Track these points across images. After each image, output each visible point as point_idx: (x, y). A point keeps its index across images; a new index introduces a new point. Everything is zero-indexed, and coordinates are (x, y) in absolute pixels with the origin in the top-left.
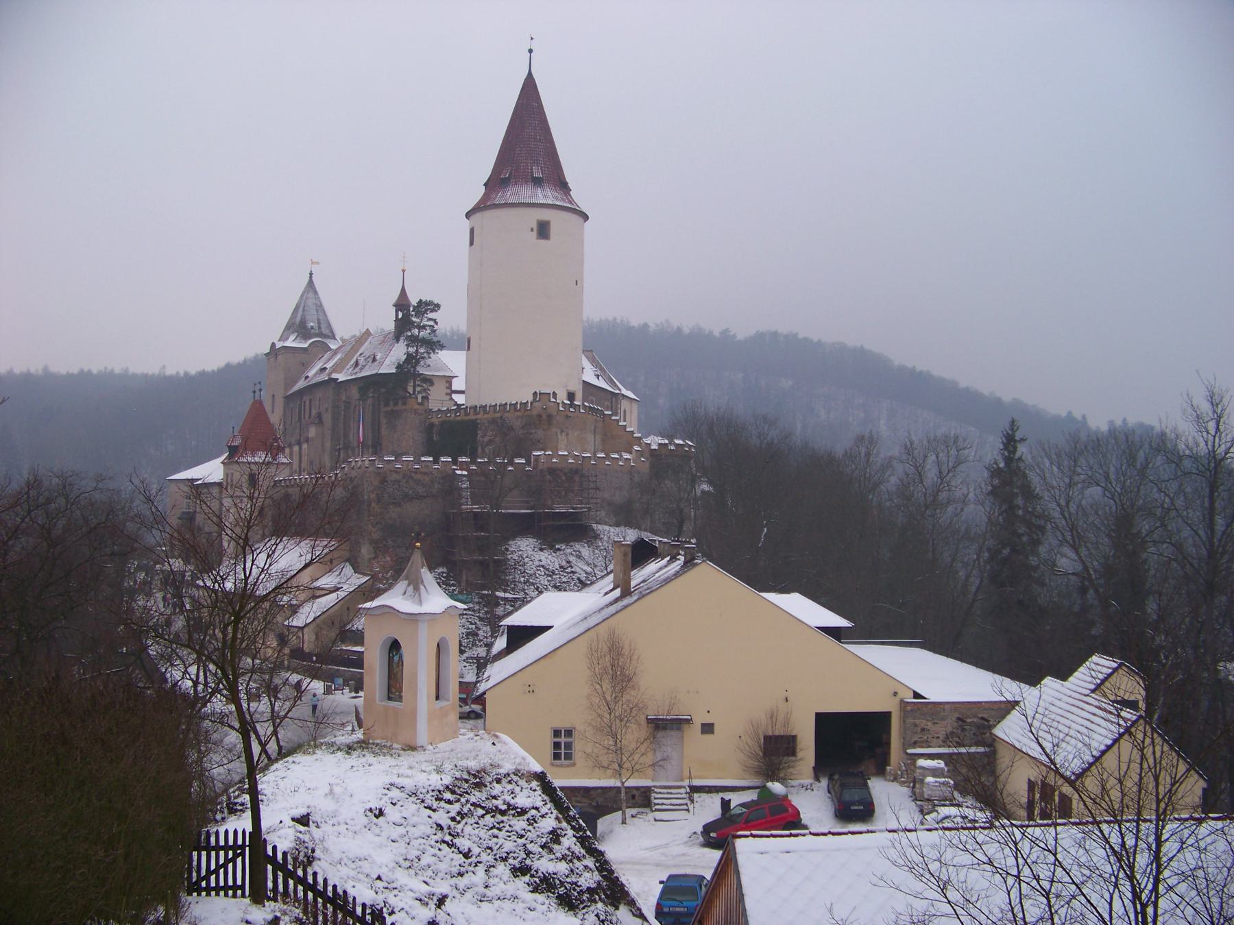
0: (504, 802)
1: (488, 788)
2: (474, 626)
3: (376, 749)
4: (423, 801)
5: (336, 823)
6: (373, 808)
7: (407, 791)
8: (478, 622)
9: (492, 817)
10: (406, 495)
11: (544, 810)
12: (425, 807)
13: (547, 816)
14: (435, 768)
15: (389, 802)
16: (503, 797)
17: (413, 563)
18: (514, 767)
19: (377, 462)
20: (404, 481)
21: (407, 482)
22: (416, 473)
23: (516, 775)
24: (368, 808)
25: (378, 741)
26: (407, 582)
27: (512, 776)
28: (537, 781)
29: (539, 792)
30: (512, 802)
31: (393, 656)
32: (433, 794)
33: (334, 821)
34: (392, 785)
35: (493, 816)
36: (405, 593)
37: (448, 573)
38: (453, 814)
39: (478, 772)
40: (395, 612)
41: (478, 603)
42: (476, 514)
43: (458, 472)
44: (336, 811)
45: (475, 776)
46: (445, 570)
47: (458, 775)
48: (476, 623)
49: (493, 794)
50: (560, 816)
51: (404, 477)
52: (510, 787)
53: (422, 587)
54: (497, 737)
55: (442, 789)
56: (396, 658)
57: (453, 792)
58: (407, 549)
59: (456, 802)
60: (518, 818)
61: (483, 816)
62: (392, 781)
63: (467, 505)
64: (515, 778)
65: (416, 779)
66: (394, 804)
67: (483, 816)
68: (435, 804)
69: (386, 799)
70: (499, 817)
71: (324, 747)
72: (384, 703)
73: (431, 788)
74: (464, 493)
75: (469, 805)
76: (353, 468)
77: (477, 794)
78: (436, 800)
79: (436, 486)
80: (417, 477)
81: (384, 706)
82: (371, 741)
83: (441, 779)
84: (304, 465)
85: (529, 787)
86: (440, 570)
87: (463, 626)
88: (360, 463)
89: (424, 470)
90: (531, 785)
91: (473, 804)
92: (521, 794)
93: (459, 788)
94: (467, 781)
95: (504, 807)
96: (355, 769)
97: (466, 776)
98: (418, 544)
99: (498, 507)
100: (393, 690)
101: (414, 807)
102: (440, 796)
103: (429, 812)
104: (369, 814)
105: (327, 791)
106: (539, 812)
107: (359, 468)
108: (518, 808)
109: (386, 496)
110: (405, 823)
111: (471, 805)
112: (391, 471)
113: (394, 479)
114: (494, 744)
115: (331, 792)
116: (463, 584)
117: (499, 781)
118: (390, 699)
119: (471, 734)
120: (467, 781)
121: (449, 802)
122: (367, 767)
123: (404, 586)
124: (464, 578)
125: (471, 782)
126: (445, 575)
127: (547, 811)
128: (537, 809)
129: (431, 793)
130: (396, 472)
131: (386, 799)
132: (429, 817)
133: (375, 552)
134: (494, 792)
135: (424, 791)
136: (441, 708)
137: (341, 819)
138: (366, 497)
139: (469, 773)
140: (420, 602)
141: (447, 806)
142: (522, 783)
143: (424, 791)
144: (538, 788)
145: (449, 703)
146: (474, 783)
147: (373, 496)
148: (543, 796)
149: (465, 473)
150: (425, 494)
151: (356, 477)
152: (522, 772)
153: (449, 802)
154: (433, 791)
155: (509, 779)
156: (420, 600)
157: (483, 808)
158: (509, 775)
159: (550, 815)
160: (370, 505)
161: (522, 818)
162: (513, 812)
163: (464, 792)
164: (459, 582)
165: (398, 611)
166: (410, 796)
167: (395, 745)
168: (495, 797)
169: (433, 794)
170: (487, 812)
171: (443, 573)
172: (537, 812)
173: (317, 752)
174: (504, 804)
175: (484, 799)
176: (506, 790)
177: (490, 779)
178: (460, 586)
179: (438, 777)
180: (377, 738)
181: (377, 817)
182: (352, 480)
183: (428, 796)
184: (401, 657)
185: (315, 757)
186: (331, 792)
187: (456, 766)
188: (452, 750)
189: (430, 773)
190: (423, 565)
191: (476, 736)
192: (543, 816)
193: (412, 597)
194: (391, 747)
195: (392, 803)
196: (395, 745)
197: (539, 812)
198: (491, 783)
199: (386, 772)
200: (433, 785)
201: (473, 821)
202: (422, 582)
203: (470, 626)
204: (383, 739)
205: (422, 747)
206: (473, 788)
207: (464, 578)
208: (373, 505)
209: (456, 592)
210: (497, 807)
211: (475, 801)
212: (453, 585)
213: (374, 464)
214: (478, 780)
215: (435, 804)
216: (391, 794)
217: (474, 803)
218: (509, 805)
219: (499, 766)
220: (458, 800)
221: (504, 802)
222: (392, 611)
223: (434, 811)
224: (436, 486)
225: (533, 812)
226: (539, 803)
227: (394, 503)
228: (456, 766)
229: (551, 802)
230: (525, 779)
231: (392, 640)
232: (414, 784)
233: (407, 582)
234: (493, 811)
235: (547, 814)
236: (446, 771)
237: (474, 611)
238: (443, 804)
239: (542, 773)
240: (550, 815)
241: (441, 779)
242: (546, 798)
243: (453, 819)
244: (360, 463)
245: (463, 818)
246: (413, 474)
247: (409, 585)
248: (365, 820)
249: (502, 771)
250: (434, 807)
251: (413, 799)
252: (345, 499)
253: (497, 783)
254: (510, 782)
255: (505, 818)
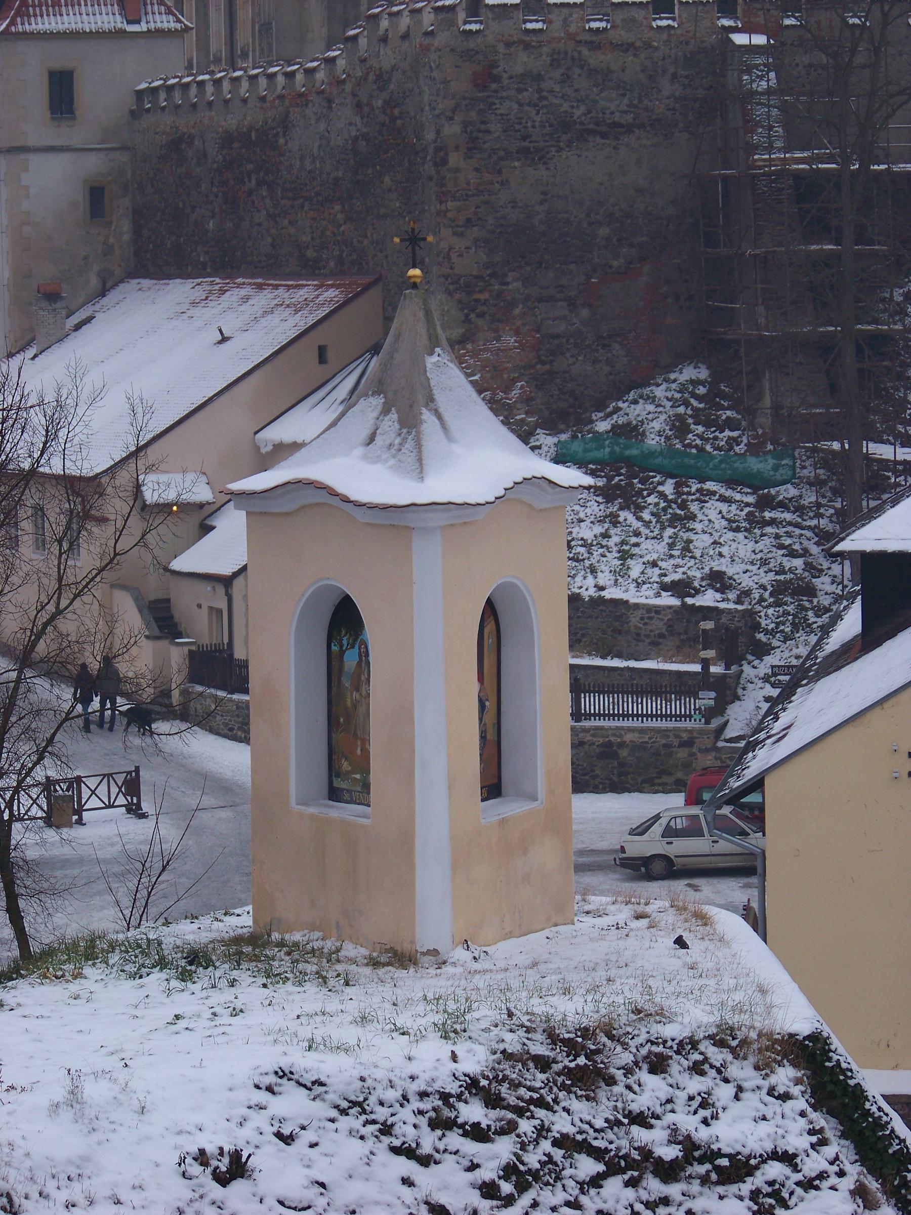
0: (675, 1136)
1: (619, 1089)
2: (798, 563)
3: (282, 963)
4: (386, 1130)
5: (79, 1198)
6: (211, 1149)
7: (331, 1097)
8: (814, 550)
9: (627, 1184)
10: (565, 125)
11: (813, 1164)
12: (396, 1150)
13: (825, 1184)
14: (439, 1018)
15: (269, 1130)
16: (669, 1118)
17: (398, 336)
18: (714, 1018)
19: (461, 15)
20: (557, 74)
21: (566, 79)
22: (594, 47)
23: (720, 1044)
24: (194, 1149)
25: (297, 937)
26: (377, 402)
27: (708, 1048)
28: (795, 1065)
29: (801, 1104)
30: (702, 1134)
31: (342, 652)
32: (423, 1106)
33: (76, 1192)
34: (282, 1074)
35: (632, 1183)
36: (371, 439)
37: (713, 383)
38: (488, 1173)
39: (585, 1032)
40: (335, 501)
41: (816, 483)
42: (798, 176)
43: (740, 39)
44: (86, 1159)
45: (572, 1048)
46: (703, 373)
47: (513, 1042)
48: (806, 552)
49: (635, 1107)
50: (873, 1185)
51: (555, 63)
52: (695, 1085)
53: (427, 416)
54: (703, 919)
55: (453, 1088)
56: (351, 659)
57: (493, 1101)
58: (572, 305)
59: (502, 1132)
60: (720, 1189)
61: (596, 1181)
62: (285, 1063)
63: (770, 149)
64: (717, 1055)
65: (366, 1056)
66: (287, 1139)
67: (596, 1181)
68: (428, 1141)
69: (259, 1120)
70: (654, 1186)
71: (114, 958)
72: (312, 810)
73: (414, 1088)
74: (761, 111)
75: (546, 1145)
76: (384, 40)
77: (578, 1106)
78: (434, 1124)
79: (667, 88)
80: (597, 59)
81: (313, 817)
82: (275, 936)
83: (454, 1057)
84: (244, 36)
85: (766, 1084)
86: (688, 373)
87: (764, 562)
88: (405, 21)
89: (621, 36)
90: (773, 1079)
91: (562, 1141)
92: (736, 1109)
93: (515, 1085)
94: (543, 1064)
95: (669, 1153)
96: (182, 1024)
97: (539, 1048)
98: (416, 272)
99: (868, 158)
100: (346, 766)
101: (358, 1148)
102: (446, 1113)
103: (405, 1166)
104: (195, 1169)
105: (59, 1094)
106: (796, 1169)
107: (405, 37)
108: (719, 1154)
109: (496, 127)
110: (321, 1202)
111: (556, 1143)
112: (508, 45)
113: (519, 69)
114: (680, 942)
115: (74, 1097)
116: (765, 421)
117: (658, 1065)
118: (334, 794)
119: (623, 914)
120: (543, 1064)
121: (477, 1133)
122: (225, 1019)
123: (372, 415)
124: (767, 401)
125: (556, 1067)
126: (701, 390)
127: (825, 1166)
128: (788, 1159)
129: (416, 1104)
130: (527, 46)
131: (259, 1120)
132: (407, 1182)
133: (467, 320)
134: (640, 1103)
135: (392, 1095)
136: (503, 822)
137: (99, 1186)
138: (430, 135)
139: (553, 1037)
140: (420, 470)
141: (470, 1147)
142: (744, 1072)
143: (392, 1095)
144: (796, 1090)
145: (535, 804)
146: (567, 1072)
147: (452, 130)
148: (813, 1115)
149: (760, 40)
150: (629, 118)
151: (394, 68)
152: (740, 1035)
153: (477, 1133)
154: (423, 1095)
155: (697, 1057)
156: (420, 460)
157: (597, 1154)
158: (694, 1044)
159: (833, 1180)
160: (445, 162)
161: (733, 1188)
162: (702, 1169)
163: (531, 1101)
164: (750, 413)
165: (346, 500)
166: (344, 1112)
167: (350, 950)
168: (641, 1120)
169: (426, 1105)
170: (612, 1170)
171: (695, 383)
172: (788, 1171)
173: (88, 971)
174: (673, 1140)
175: (599, 1123)
176: (682, 1096)
177: (627, 1058)
178: (752, 426)
179: (444, 1049)
180: (289, 930)
181: (223, 1179)
182: (382, 79)
183: (406, 1114)
184: (364, 655)
185: (75, 987)
186: (74, 1097)
187: (510, 1015)
188: (535, 964)
189: (420, 1037)
190: (433, 343)
191: (638, 917)
192: (809, 1185)
193: (394, 449)
194: (333, 957)
195: (279, 1135)
196: (350, 950)
197: (796, 1169)
198: (628, 1071)
199: (277, 1036)
200: (424, 1078)
201: (560, 1197)
202: (430, 399)
203: (788, 563)
204: (313, 928)
205: (435, 952)
206: (563, 1088)
207: (767, 401)
208: (454, 159)
209: (740, 449)
210: (646, 1153)
211: (569, 1129)
212: (730, 424)
213: (453, 23)
214: (582, 1060)
215: (428, 1141)
216: (278, 1106)
217: (565, 1136)
218: (689, 1145)
219: (662, 1015)
220: (509, 1128)
221: (675, 1136)
222: (323, 497)
223: (425, 1161)
224: (667, 88)
225: (775, 1170)
226: (797, 1142)
227: (525, 152)
228: (510, 1015)
229: (843, 1135)
230: (752, 1059)
231: (334, 600)
232: (356, 1074)
233: (377, 402)
234: (631, 1164)
235: (822, 1176)
236: (474, 1029)
237: (800, 509)
238: (454, 1139)
239: (815, 1037)
240: (833, 1180)
241: (454, 1057)
242: (820, 1120)
243: (488, 1190)
244: (405, 21)
245: (522, 1187)
246: (586, 52)
247: (385, 411)
248: (180, 1191)
249: (671, 1031)
250: (426, 1148)
251: (354, 1121)
252: (362, 145)
253: (653, 1071)
254: (697, 1069)
255: (674, 1190)
